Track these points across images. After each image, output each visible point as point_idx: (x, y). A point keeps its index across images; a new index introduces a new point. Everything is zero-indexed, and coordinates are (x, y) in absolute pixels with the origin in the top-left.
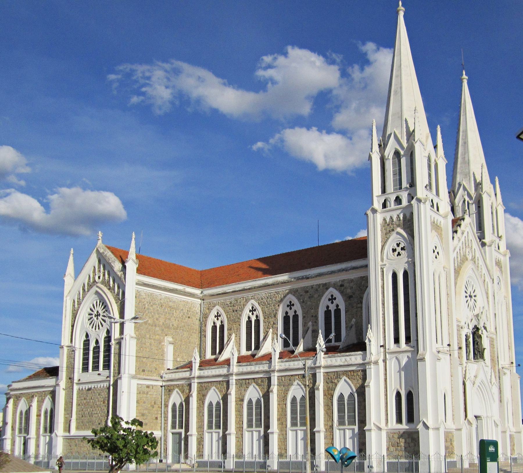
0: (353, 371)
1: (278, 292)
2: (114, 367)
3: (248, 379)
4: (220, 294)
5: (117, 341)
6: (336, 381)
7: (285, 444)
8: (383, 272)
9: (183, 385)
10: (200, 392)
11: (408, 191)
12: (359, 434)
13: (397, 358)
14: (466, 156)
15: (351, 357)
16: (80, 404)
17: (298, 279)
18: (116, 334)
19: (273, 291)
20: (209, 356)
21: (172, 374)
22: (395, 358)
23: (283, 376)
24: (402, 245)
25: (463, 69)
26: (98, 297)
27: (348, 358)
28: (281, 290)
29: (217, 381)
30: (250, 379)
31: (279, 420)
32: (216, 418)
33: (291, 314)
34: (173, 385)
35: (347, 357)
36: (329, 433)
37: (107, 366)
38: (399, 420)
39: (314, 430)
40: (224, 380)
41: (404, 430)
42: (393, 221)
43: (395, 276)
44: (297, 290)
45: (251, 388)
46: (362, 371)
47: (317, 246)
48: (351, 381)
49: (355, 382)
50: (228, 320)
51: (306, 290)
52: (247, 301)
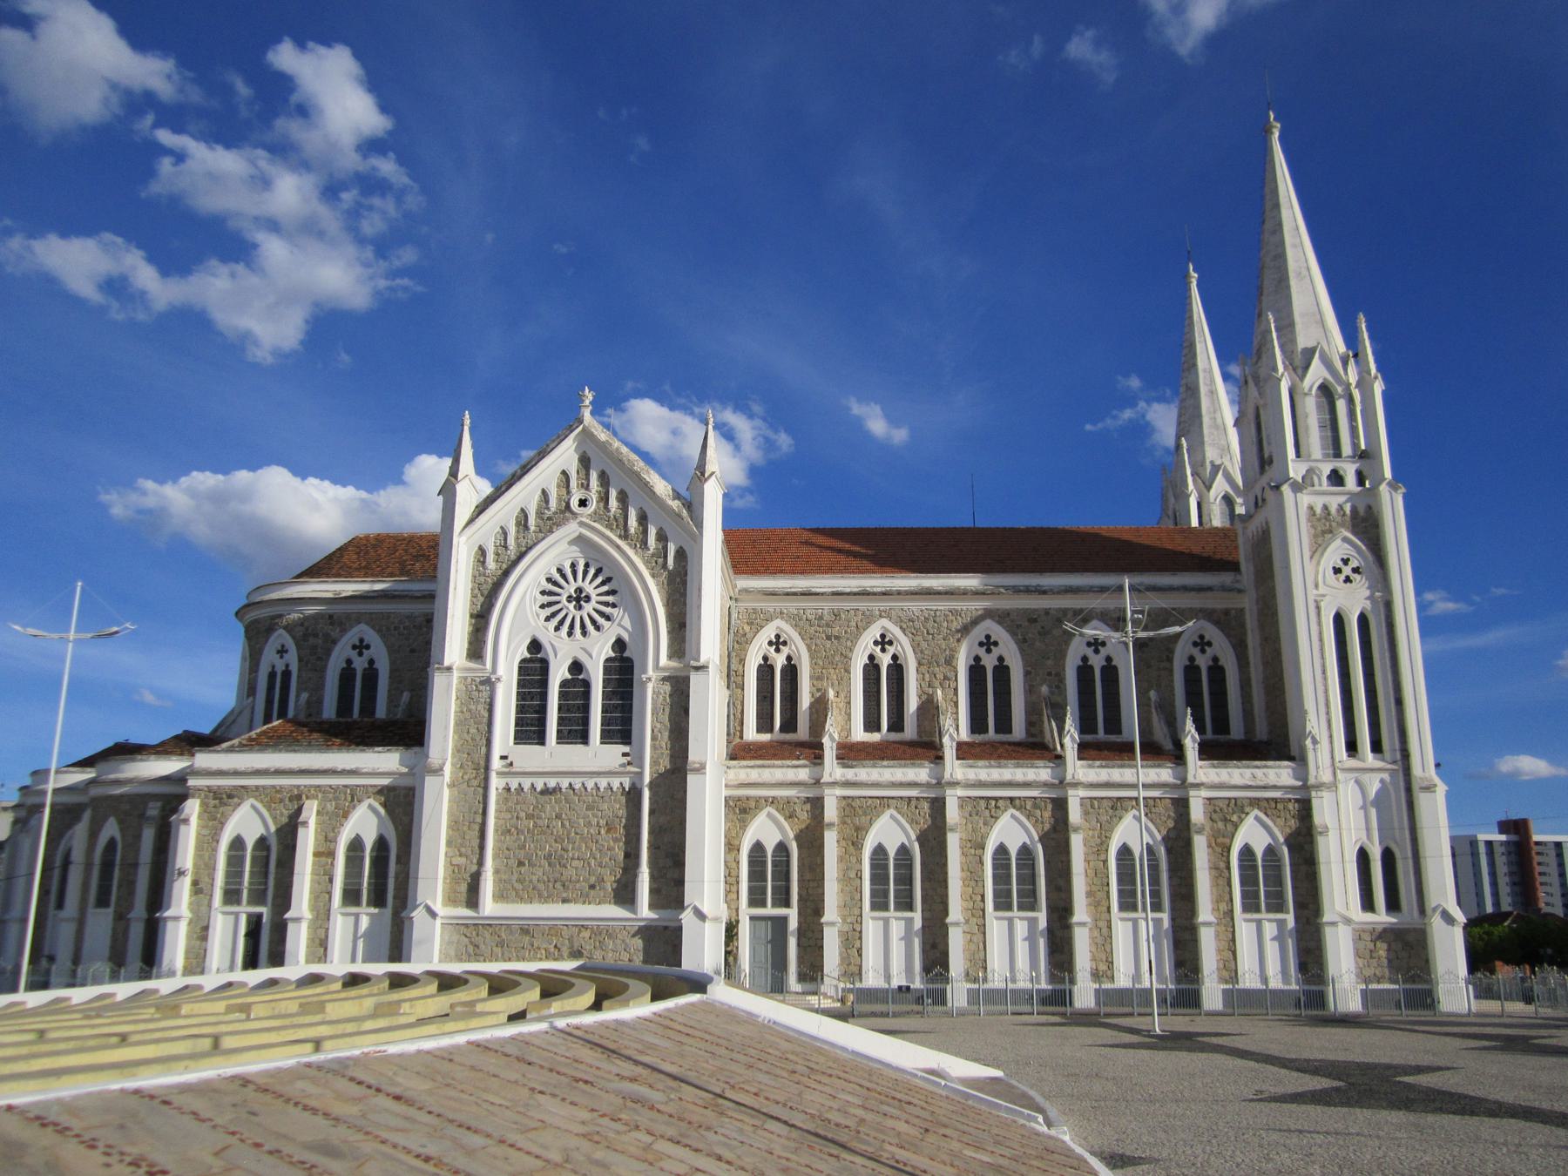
0: (1276, 800)
1: (957, 611)
2: (654, 738)
3: (996, 799)
4: (795, 594)
5: (667, 674)
6: (1235, 818)
7: (1109, 950)
8: (1318, 608)
9: (788, 801)
10: (846, 819)
11: (1358, 465)
12: (1297, 932)
13: (1357, 782)
14: (1218, 415)
15: (1265, 770)
16: (509, 831)
17: (1017, 590)
18: (657, 660)
19: (942, 608)
20: (751, 733)
21: (749, 770)
22: (1353, 781)
23: (1095, 798)
24: (1354, 563)
25: (1189, 260)
26: (581, 552)
27: (1259, 773)
28: (965, 608)
29: (901, 798)
30: (1001, 798)
31: (1089, 894)
32: (895, 884)
33: (989, 662)
34: (758, 800)
35: (1257, 770)
36: (1224, 928)
37: (1377, 747)
38: (1368, 904)
39: (287, 916)
40: (925, 795)
41: (1385, 926)
42: (1329, 514)
43: (1339, 621)
44: (1008, 614)
45: (1249, 821)
46: (1175, 802)
47: (972, 526)
48: (1272, 820)
49: (1281, 822)
50: (812, 658)
51: (1032, 617)
52: (869, 619)
